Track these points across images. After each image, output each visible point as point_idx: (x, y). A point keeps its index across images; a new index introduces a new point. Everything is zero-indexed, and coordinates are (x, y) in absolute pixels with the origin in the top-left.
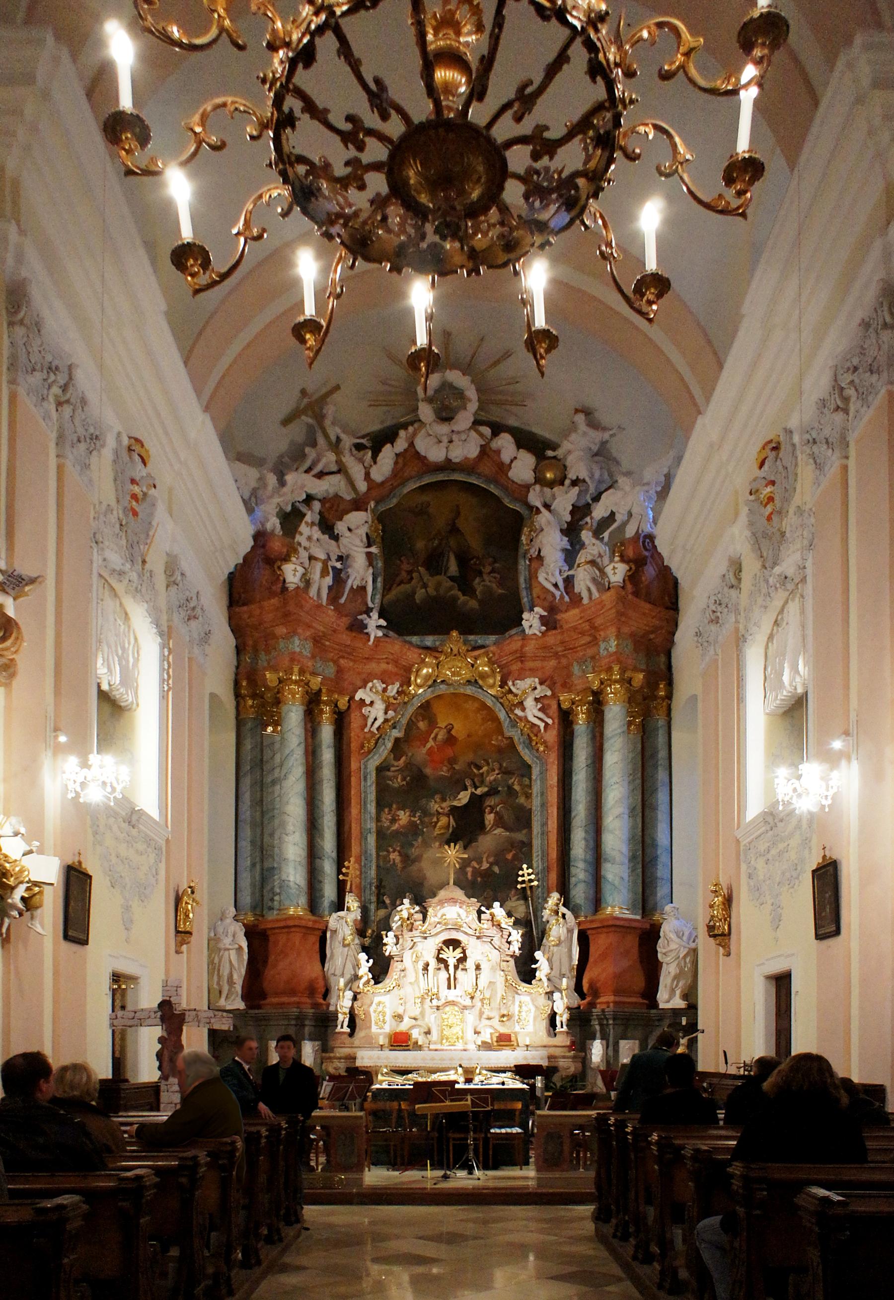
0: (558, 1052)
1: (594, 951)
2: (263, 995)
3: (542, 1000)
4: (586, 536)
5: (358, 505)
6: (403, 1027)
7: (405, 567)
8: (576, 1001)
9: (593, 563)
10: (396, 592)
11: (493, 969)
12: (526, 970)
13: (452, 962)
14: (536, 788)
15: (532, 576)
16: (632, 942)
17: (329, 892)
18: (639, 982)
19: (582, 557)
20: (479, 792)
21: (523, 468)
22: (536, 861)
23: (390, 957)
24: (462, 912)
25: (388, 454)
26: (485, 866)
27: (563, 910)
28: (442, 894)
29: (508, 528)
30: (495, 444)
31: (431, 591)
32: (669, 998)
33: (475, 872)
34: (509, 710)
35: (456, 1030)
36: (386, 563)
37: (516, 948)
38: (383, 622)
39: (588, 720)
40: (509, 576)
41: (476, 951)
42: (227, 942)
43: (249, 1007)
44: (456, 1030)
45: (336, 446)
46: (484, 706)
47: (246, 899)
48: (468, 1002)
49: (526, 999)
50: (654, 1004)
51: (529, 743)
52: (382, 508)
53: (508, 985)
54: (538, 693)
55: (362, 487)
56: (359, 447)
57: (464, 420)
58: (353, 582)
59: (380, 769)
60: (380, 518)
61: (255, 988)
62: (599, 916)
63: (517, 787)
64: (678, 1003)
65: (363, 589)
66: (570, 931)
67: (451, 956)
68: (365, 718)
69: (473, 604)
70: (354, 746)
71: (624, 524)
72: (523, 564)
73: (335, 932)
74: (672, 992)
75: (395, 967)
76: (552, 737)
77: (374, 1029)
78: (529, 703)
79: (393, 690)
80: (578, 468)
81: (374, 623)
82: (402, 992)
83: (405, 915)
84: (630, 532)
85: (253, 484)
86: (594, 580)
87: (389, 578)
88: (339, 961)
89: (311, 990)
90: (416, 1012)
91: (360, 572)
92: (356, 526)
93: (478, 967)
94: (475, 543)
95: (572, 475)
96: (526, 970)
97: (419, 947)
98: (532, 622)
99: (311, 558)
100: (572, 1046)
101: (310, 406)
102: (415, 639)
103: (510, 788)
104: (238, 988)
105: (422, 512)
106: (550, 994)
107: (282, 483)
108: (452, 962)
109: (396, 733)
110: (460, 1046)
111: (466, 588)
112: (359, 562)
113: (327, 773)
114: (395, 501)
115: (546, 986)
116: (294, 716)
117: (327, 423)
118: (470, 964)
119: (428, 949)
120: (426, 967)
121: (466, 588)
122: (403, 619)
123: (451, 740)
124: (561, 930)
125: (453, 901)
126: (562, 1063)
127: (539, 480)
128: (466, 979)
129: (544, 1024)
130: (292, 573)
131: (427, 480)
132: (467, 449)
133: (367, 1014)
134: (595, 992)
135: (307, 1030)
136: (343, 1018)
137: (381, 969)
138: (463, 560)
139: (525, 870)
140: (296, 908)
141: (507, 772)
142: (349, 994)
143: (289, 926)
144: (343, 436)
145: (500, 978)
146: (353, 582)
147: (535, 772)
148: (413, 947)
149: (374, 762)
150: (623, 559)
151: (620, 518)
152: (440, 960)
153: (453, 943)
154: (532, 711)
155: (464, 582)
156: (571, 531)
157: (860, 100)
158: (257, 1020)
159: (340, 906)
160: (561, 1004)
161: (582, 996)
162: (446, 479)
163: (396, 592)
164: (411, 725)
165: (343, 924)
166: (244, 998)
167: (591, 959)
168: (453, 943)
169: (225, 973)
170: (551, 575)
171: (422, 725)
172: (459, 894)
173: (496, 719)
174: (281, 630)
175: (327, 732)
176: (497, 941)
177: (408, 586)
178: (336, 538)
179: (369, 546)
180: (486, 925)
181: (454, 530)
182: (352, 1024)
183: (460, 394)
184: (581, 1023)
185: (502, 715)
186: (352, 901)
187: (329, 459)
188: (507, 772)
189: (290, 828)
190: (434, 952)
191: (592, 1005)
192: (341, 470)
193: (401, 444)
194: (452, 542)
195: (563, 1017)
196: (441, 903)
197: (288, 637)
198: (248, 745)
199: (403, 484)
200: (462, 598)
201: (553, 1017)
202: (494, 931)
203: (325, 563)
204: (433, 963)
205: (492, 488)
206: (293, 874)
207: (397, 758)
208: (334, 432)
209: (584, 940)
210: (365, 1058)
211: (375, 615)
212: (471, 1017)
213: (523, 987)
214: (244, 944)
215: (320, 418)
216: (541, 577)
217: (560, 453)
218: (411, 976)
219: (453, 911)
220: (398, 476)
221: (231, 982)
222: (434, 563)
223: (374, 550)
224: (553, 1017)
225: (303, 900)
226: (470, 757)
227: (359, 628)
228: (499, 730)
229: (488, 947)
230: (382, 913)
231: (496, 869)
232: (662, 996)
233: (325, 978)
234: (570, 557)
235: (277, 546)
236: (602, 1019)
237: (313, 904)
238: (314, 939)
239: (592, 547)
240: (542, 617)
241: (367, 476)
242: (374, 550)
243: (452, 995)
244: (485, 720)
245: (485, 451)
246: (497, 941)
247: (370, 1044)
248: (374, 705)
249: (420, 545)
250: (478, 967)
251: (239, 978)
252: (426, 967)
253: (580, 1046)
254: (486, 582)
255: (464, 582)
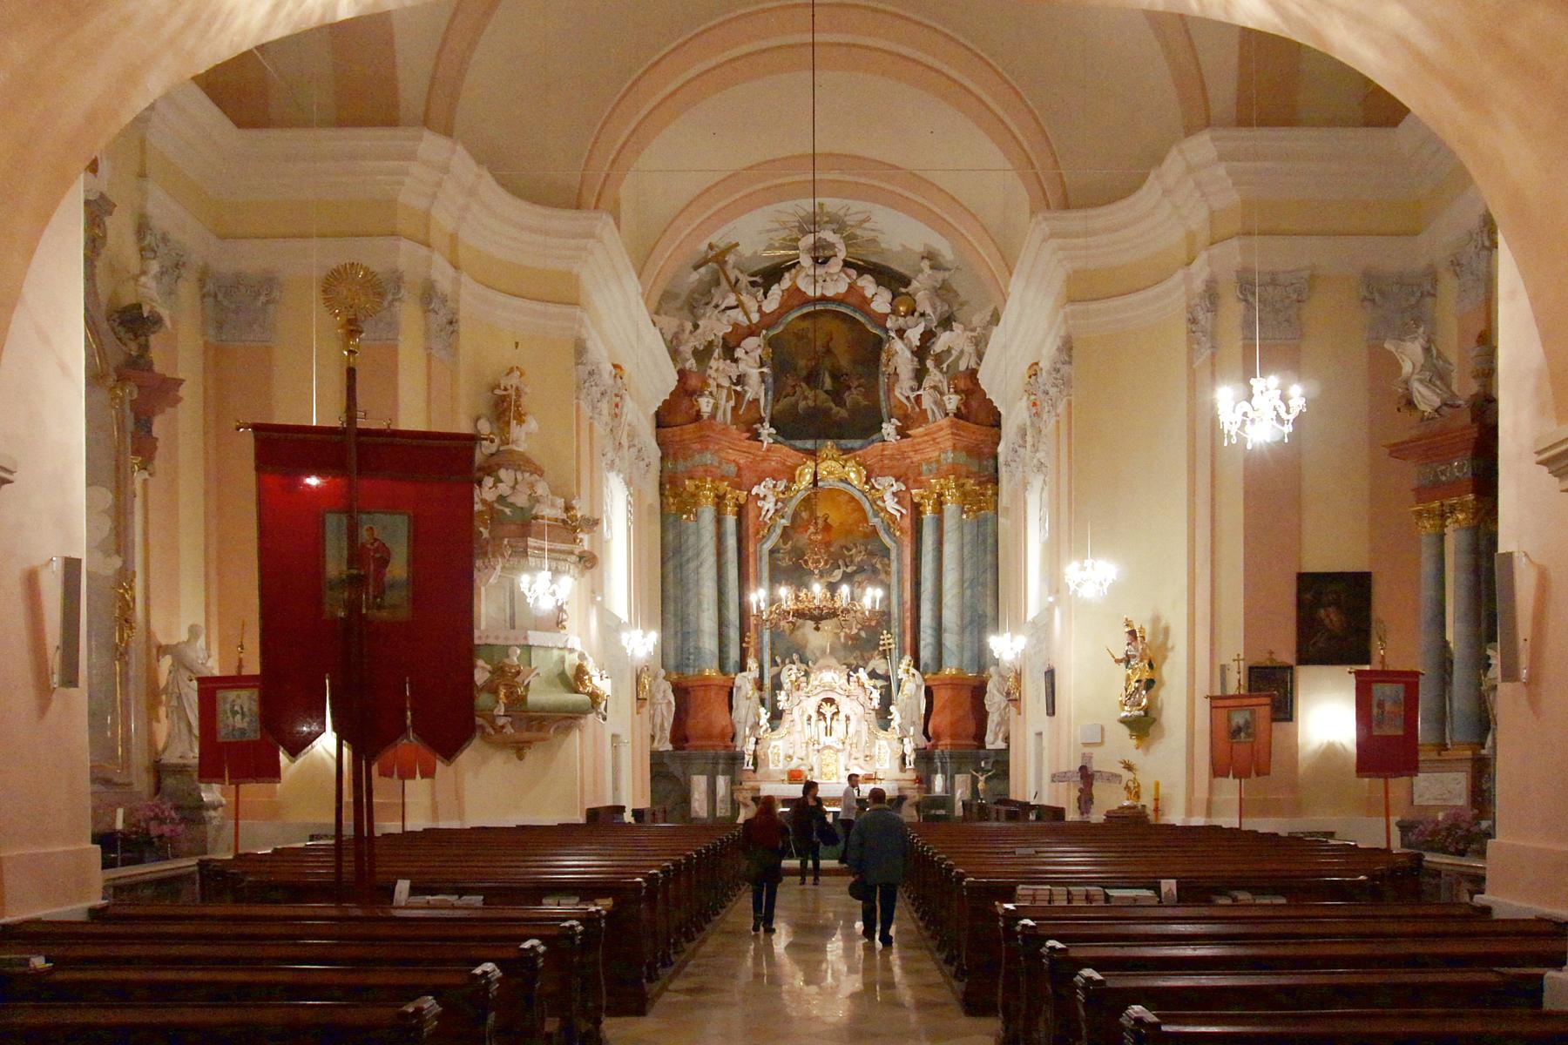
0: (908, 784)
1: (937, 703)
2: (686, 739)
3: (896, 744)
4: (930, 363)
5: (752, 331)
6: (794, 765)
7: (791, 382)
8: (923, 742)
9: (935, 388)
10: (785, 402)
11: (859, 721)
12: (883, 715)
13: (828, 716)
14: (894, 567)
15: (890, 390)
16: (966, 696)
17: (734, 654)
18: (971, 728)
19: (927, 383)
20: (849, 570)
21: (881, 302)
22: (895, 630)
23: (783, 711)
24: (836, 677)
25: (776, 291)
26: (855, 631)
27: (913, 670)
28: (821, 662)
29: (871, 350)
30: (860, 283)
31: (811, 403)
32: (993, 742)
33: (847, 636)
34: (873, 502)
35: (832, 768)
36: (775, 382)
37: (876, 703)
38: (773, 431)
39: (934, 511)
40: (871, 391)
41: (846, 707)
42: (659, 696)
43: (676, 748)
44: (832, 768)
45: (735, 286)
46: (852, 499)
47: (672, 662)
48: (840, 746)
49: (883, 743)
50: (982, 745)
51: (888, 530)
52: (772, 333)
53: (870, 733)
54: (894, 489)
55: (755, 318)
56: (753, 284)
57: (835, 266)
58: (749, 396)
59: (772, 552)
60: (771, 343)
61: (680, 735)
62: (941, 675)
63: (879, 566)
64: (1001, 745)
65: (757, 401)
66: (918, 687)
67: (828, 710)
68: (760, 509)
69: (843, 413)
70: (751, 531)
71: (959, 358)
72: (883, 380)
73: (739, 688)
74: (996, 735)
75: (787, 718)
76: (907, 523)
77: (771, 766)
78: (888, 497)
79: (782, 485)
80: (924, 305)
81: (766, 431)
82: (792, 738)
83: (793, 678)
84: (962, 367)
85: (674, 330)
86: (935, 403)
87: (777, 392)
88: (743, 712)
89: (722, 735)
90: (803, 754)
91: (755, 389)
92: (753, 346)
93: (848, 718)
94: (844, 362)
95: (920, 309)
96: (883, 715)
97: (804, 704)
98: (889, 429)
99: (718, 386)
100: (919, 780)
101: (716, 256)
102: (798, 443)
103: (873, 566)
104: (668, 734)
105: (800, 336)
106: (901, 740)
107: (696, 326)
108: (828, 716)
109: (785, 522)
110: (834, 780)
111: (840, 402)
112: (754, 373)
113: (731, 542)
114: (781, 328)
115: (898, 734)
116: (707, 514)
117: (729, 268)
118: (842, 716)
119: (811, 705)
120: (809, 718)
121: (840, 402)
122: (791, 426)
123: (827, 528)
124: (910, 688)
125: (829, 667)
126: (908, 793)
127: (894, 312)
128: (839, 727)
129: (897, 763)
130: (705, 405)
131: (805, 310)
132: (837, 285)
133: (766, 755)
134: (938, 736)
135: (721, 767)
136: (748, 758)
137: (776, 716)
138: (835, 377)
139: (885, 634)
140: (711, 671)
141: (871, 554)
142: (753, 740)
143: (706, 684)
144: (741, 276)
145: (864, 726)
146: (749, 396)
147: (893, 555)
148: (800, 706)
149: (768, 546)
150: (956, 392)
151: (955, 353)
152: (819, 713)
153: (831, 701)
154: (891, 504)
155: (837, 396)
156: (921, 352)
157: (1044, 240)
158: (683, 758)
159: (743, 667)
160: (909, 748)
161: (929, 739)
162: (821, 310)
163: (785, 402)
164: (796, 515)
165: (745, 682)
166: (672, 741)
167: (935, 709)
168: (831, 701)
169: (658, 721)
170: (903, 390)
171: (805, 515)
172: (833, 662)
173: (862, 510)
174: (697, 446)
175: (730, 521)
176: (862, 699)
177: (793, 399)
178: (735, 361)
179: (762, 365)
180: (853, 686)
181: (828, 351)
182: (755, 763)
183: (832, 246)
184: (925, 758)
185: (867, 506)
186: (752, 663)
187: (731, 300)
188: (871, 554)
189: (705, 606)
190: (815, 707)
191: (935, 746)
192: (739, 305)
193: (786, 282)
194: (827, 362)
195: (911, 757)
196: (820, 669)
197: (701, 451)
198: (670, 537)
199: (788, 312)
200: (835, 409)
201: (903, 757)
202: (859, 691)
203: (729, 389)
204: (815, 716)
205: (858, 316)
206: (709, 644)
207: (785, 543)
208: (733, 275)
209: (929, 693)
210: (767, 789)
211: (767, 425)
212: (842, 758)
213: (882, 734)
214: (672, 699)
215: (722, 263)
216: (897, 393)
217: (910, 289)
218: (798, 727)
219: (830, 677)
220: (784, 308)
221: (662, 728)
222: (812, 378)
223: (765, 370)
224: (903, 757)
225: (716, 664)
226: (842, 542)
227: (756, 436)
228: (866, 519)
229: (855, 703)
230: (776, 669)
231: (863, 634)
232: (989, 738)
233: (733, 725)
234: (920, 375)
235: (693, 382)
236: (942, 758)
237: (722, 667)
238: (724, 694)
239: (934, 376)
240: (897, 428)
241: (760, 309)
242: (765, 370)
243: (828, 741)
244: (854, 511)
245: (851, 287)
246: (862, 699)
247: (769, 778)
248: (767, 496)
249: (802, 363)
250: (848, 718)
251: (668, 726)
252: (809, 718)
253: (924, 781)
254: (853, 396)
255: (837, 396)
